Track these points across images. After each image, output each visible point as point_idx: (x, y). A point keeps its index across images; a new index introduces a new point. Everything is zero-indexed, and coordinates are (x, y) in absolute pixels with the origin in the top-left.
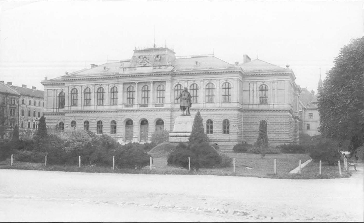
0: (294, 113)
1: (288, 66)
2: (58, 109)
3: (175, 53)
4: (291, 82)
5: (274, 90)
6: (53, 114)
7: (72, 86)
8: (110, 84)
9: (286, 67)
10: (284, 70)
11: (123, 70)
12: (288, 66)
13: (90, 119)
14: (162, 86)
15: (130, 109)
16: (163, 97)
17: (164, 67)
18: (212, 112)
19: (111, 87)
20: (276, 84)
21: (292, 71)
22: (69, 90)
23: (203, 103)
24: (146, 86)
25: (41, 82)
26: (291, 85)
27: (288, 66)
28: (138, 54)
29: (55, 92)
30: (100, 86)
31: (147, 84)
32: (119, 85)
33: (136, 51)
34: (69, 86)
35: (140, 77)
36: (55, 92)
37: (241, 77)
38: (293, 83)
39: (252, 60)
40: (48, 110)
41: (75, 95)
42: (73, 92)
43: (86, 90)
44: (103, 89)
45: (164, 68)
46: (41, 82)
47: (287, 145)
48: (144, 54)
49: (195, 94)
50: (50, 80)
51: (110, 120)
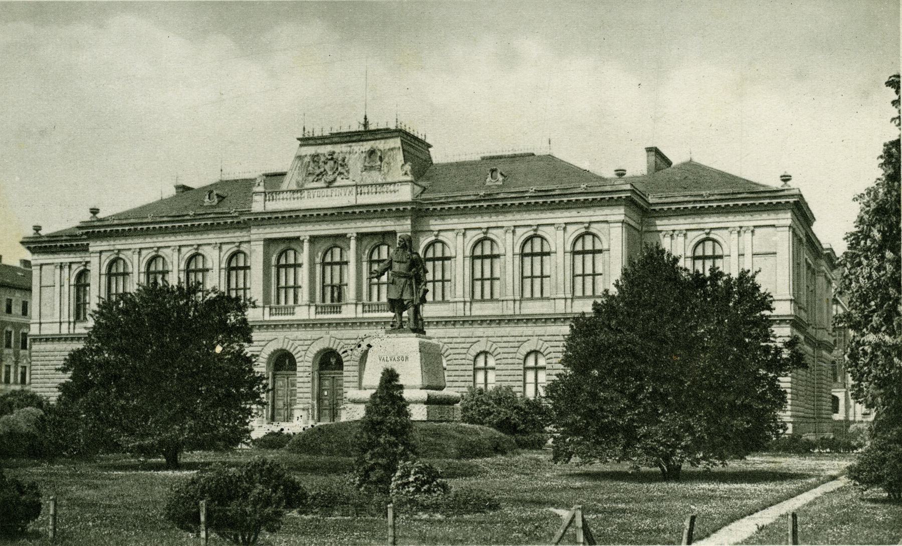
0: (810, 330)
1: (786, 179)
2: (75, 323)
3: (429, 146)
4: (798, 232)
5: (743, 255)
6: (59, 339)
7: (110, 251)
8: (225, 243)
9: (783, 183)
10: (774, 193)
11: (265, 200)
12: (786, 179)
13: (546, 345)
14: (337, 251)
15: (280, 321)
16: (443, 281)
17: (392, 187)
18: (539, 329)
19: (476, 239)
20: (748, 235)
21: (801, 195)
22: (100, 264)
23: (566, 299)
24: (291, 249)
25: (22, 243)
26: (800, 240)
27: (789, 180)
28: (310, 150)
29: (66, 270)
30: (194, 251)
31: (293, 245)
32: (253, 248)
33: (305, 141)
34: (101, 252)
35: (330, 218)
36: (66, 270)
37: (636, 217)
38: (807, 235)
39: (674, 164)
40: (43, 325)
41: (121, 279)
42: (528, 250)
43: (329, 255)
44: (164, 263)
45: (385, 190)
46: (22, 243)
47: (24, 427)
48: (325, 150)
49: (529, 271)
50: (48, 236)
51: (309, 354)
